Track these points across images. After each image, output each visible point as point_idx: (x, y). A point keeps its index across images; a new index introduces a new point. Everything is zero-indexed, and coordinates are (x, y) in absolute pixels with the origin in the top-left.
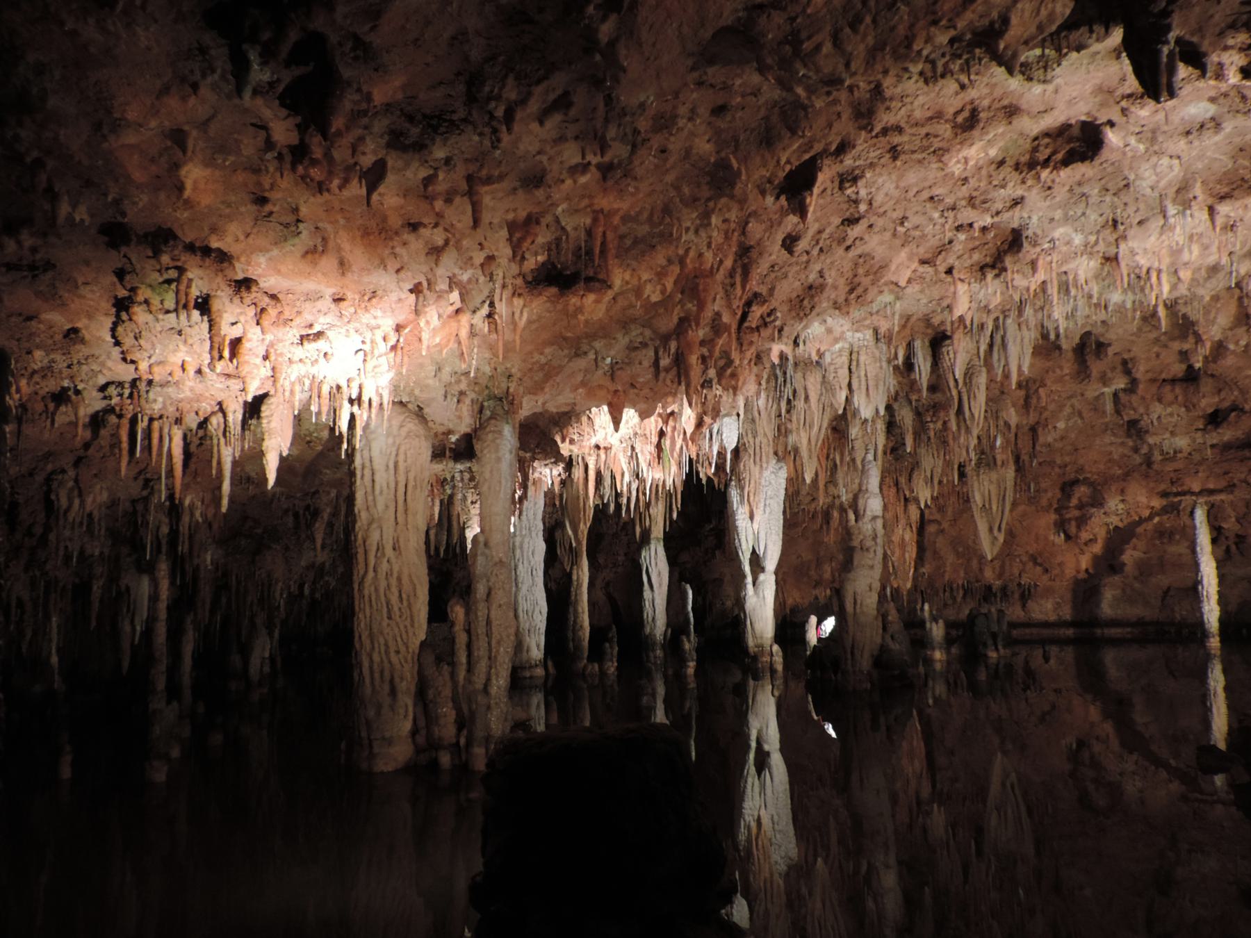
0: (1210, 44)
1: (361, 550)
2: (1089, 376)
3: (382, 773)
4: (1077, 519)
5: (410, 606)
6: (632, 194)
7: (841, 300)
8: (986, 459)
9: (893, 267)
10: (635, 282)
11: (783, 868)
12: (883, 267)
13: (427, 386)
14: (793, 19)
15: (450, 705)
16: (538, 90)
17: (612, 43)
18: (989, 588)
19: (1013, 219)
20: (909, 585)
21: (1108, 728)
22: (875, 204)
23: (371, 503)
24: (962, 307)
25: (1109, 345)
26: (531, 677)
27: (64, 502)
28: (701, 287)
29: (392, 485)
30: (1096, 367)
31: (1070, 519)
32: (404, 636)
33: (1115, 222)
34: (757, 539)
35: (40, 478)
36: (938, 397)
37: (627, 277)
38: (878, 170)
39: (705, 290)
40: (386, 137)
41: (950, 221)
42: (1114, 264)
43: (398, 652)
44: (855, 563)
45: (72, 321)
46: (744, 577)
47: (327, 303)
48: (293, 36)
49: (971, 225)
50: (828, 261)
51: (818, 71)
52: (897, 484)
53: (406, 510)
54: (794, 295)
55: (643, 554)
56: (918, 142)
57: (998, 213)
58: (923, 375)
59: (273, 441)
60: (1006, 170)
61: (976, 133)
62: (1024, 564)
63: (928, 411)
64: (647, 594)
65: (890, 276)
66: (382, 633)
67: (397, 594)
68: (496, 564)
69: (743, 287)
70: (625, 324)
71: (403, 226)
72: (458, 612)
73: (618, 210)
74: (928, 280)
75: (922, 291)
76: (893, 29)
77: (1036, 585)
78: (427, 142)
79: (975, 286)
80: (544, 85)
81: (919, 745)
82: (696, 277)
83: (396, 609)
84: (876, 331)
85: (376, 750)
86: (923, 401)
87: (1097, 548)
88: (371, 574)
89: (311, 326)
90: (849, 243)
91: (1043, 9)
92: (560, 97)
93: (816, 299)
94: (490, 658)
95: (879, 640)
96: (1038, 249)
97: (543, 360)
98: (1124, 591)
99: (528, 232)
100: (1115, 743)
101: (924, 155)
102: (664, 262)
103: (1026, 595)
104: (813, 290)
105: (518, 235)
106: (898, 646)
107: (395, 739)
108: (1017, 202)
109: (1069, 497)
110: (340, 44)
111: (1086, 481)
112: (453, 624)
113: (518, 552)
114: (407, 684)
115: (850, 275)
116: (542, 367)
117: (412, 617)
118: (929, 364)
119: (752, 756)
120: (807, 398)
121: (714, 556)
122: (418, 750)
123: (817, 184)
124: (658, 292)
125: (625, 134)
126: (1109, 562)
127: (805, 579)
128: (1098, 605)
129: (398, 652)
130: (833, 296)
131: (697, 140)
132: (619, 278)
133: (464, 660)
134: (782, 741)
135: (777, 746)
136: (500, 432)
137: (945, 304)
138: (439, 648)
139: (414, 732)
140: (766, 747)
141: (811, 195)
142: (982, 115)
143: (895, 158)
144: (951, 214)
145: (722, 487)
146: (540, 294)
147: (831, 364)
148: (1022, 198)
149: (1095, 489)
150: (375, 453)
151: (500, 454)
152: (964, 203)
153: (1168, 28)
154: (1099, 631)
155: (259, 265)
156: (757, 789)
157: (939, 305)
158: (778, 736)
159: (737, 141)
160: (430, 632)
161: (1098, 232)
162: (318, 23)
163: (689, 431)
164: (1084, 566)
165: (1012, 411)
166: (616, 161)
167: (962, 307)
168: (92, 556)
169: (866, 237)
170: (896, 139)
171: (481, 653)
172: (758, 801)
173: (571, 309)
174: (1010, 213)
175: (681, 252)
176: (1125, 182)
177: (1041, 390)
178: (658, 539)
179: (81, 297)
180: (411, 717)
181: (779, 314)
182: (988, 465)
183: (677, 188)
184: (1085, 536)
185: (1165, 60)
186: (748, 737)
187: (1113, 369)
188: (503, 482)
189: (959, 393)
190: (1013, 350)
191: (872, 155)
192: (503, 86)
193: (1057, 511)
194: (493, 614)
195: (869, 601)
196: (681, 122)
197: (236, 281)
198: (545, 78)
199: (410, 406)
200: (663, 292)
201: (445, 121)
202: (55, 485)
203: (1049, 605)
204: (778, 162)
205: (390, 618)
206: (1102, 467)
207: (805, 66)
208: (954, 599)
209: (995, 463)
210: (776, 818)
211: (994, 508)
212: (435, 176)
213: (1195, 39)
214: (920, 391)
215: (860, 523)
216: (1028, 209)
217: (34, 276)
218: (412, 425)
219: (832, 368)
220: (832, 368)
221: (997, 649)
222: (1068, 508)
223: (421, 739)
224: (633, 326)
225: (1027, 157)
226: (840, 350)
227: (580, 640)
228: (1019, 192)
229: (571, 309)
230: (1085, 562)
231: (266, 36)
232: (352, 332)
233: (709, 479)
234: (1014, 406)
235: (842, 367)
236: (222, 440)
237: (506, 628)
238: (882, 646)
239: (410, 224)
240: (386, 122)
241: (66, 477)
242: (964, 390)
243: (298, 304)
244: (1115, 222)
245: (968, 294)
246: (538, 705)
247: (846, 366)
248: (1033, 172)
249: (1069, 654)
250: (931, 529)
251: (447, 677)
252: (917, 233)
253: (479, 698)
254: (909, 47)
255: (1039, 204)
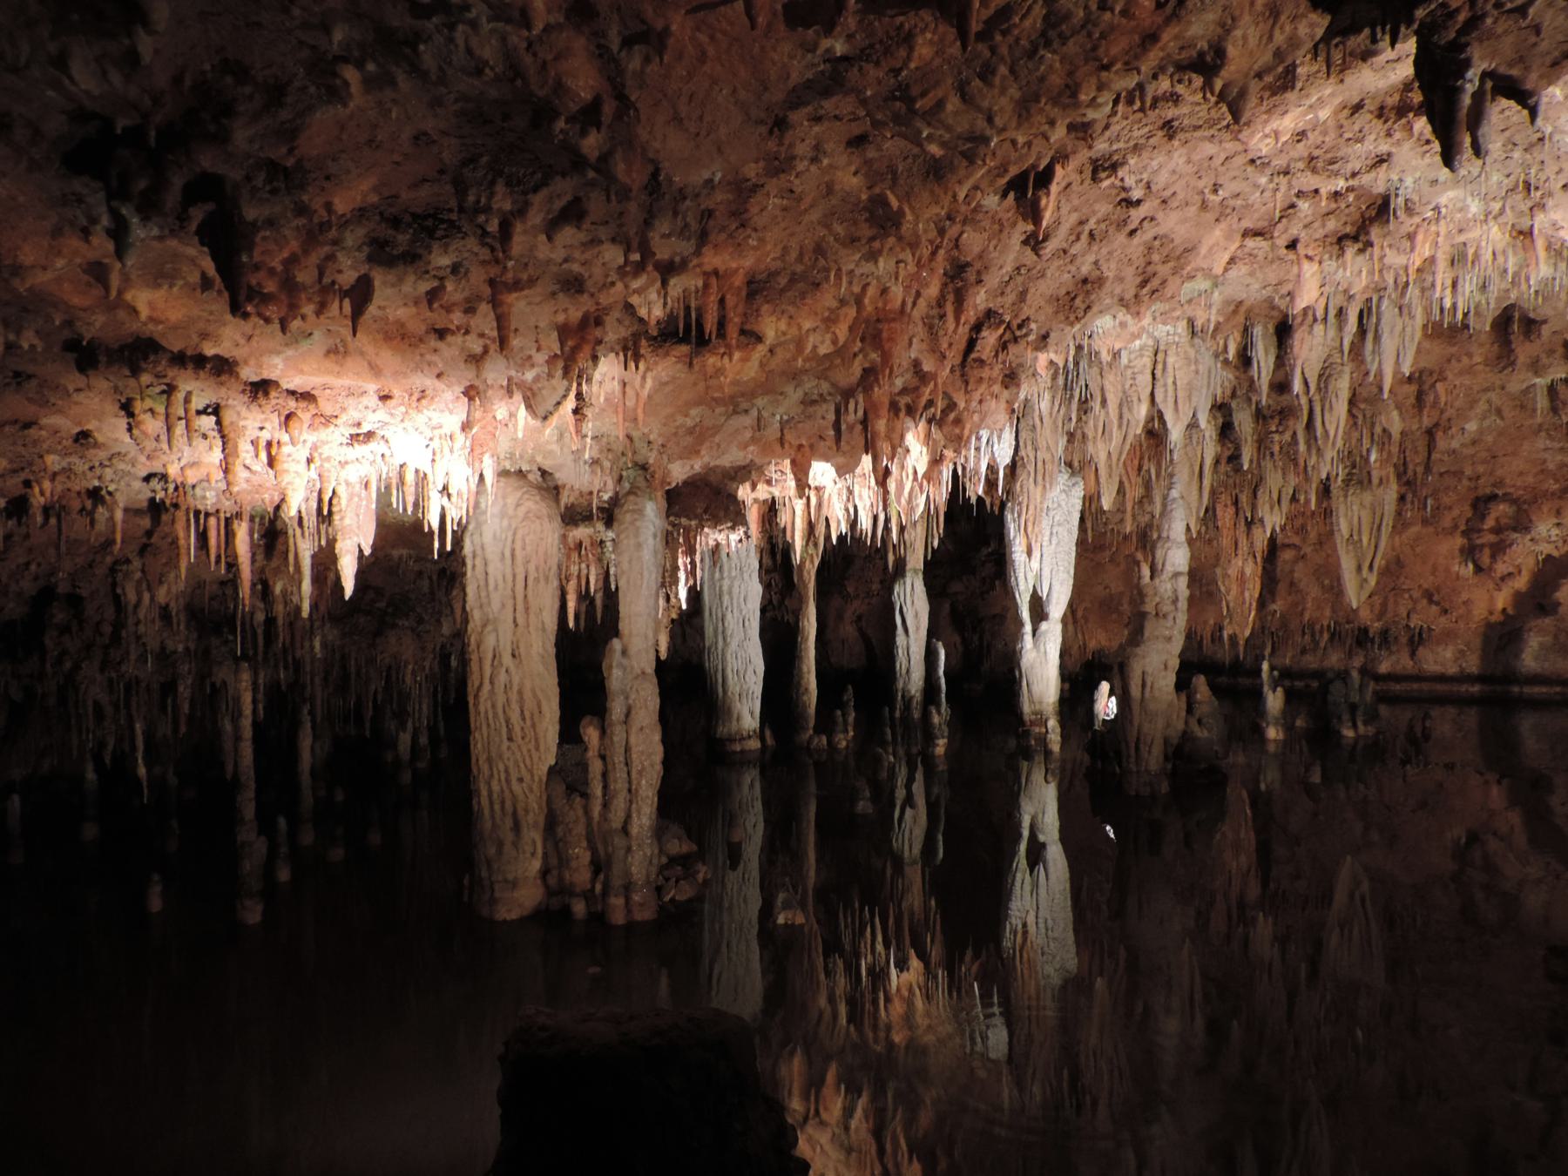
0: (1541, 77)
1: (474, 657)
2: (1513, 363)
3: (505, 921)
4: (1492, 546)
5: (534, 726)
6: (754, 248)
7: (1129, 295)
8: (1358, 476)
9: (1203, 250)
10: (794, 331)
11: (1056, 980)
12: (1189, 250)
13: (551, 452)
14: (896, 72)
15: (584, 844)
16: (537, 199)
17: (605, 158)
18: (1364, 631)
19: (1378, 182)
20: (1247, 633)
21: (1515, 818)
22: (1154, 188)
23: (484, 600)
24: (1309, 295)
25: (1545, 322)
26: (742, 752)
27: (131, 596)
28: (885, 335)
29: (509, 578)
30: (1524, 351)
31: (1483, 546)
32: (528, 762)
33: (1527, 186)
34: (1039, 576)
35: (100, 571)
36: (1285, 400)
37: (783, 326)
38: (1145, 154)
39: (890, 339)
40: (366, 249)
41: (1283, 188)
42: (1527, 241)
43: (521, 780)
44: (1147, 634)
45: (79, 424)
46: (1021, 624)
47: (372, 400)
48: (177, 182)
49: (1316, 191)
50: (1104, 251)
51: (948, 129)
52: (1236, 503)
53: (527, 609)
54: (1063, 291)
55: (896, 589)
56: (1203, 114)
57: (1354, 175)
58: (1264, 374)
59: (348, 542)
60: (1364, 118)
61: (1291, 96)
62: (1415, 602)
63: (1272, 417)
64: (900, 639)
65: (1198, 261)
66: (501, 757)
67: (518, 710)
68: (637, 678)
69: (957, 319)
70: (795, 376)
71: (427, 332)
72: (591, 734)
73: (737, 270)
74: (1261, 258)
75: (1252, 274)
76: (1042, 79)
77: (1430, 629)
78: (420, 251)
79: (1330, 265)
80: (544, 192)
81: (1248, 837)
82: (878, 320)
83: (517, 729)
84: (1191, 323)
85: (497, 895)
86: (1259, 412)
87: (1521, 583)
88: (487, 687)
89: (359, 425)
90: (1132, 227)
91: (1277, 32)
92: (570, 204)
93: (1093, 297)
94: (630, 791)
95: (1180, 726)
96: (1417, 220)
97: (689, 422)
98: (1556, 637)
99: (583, 340)
100: (1520, 839)
101: (1212, 132)
102: (835, 304)
103: (1417, 640)
104: (1089, 284)
105: (570, 343)
106: (1206, 734)
107: (520, 881)
108: (1381, 160)
109: (1483, 517)
110: (248, 178)
111: (1506, 498)
112: (586, 750)
113: (726, 598)
114: (534, 815)
115: (1141, 262)
116: (691, 431)
117: (537, 740)
118: (1272, 359)
119: (1023, 847)
120: (1104, 402)
121: (993, 588)
122: (550, 892)
123: (1055, 181)
124: (828, 342)
125: (686, 225)
126: (1538, 599)
127: (1114, 616)
128: (1517, 655)
129: (521, 780)
130: (1118, 291)
131: (839, 174)
132: (771, 328)
133: (599, 792)
134: (1062, 830)
135: (1056, 835)
136: (640, 512)
137: (1284, 291)
138: (569, 777)
139: (545, 873)
140: (1042, 838)
141: (1048, 194)
142: (1299, 70)
143: (1171, 137)
144: (1283, 180)
145: (996, 509)
146: (667, 354)
147: (1127, 367)
148: (1389, 155)
149: (1519, 509)
150: (488, 538)
151: (641, 539)
152: (1301, 165)
153: (1467, 64)
154: (1516, 689)
155: (275, 366)
156: (1027, 887)
157: (1276, 291)
158: (1057, 824)
159: (895, 174)
160: (561, 754)
161: (1504, 199)
162: (207, 160)
163: (921, 471)
164: (1500, 605)
165: (1395, 413)
166: (677, 259)
167: (1309, 295)
168: (175, 652)
169: (1160, 216)
170: (1170, 112)
171: (619, 786)
172: (1028, 903)
173: (710, 370)
174: (1373, 174)
175: (856, 289)
176: (1539, 135)
177: (1439, 386)
178: (915, 571)
179: (76, 403)
180: (540, 851)
181: (1033, 326)
182: (1360, 482)
183: (828, 227)
184: (1501, 568)
185: (1467, 100)
186: (1019, 825)
187: (1551, 352)
188: (646, 573)
189: (1310, 401)
190: (1389, 344)
191: (1136, 134)
192: (492, 195)
193: (1464, 533)
194: (633, 740)
195: (1162, 683)
196: (801, 166)
197: (252, 384)
198: (544, 183)
199: (531, 477)
200: (835, 342)
201: (442, 221)
202: (120, 576)
203: (1448, 653)
204: (954, 196)
205: (510, 739)
206: (1530, 479)
207: (929, 124)
208: (1317, 643)
209: (1370, 481)
210: (1050, 922)
211: (1365, 540)
212: (442, 288)
213: (1515, 72)
214: (1260, 394)
215: (1157, 581)
216: (1398, 169)
217: (19, 384)
218: (534, 503)
219: (1129, 372)
220: (1129, 372)
221: (1355, 726)
222: (1480, 531)
223: (552, 881)
224: (805, 378)
225: (1397, 97)
226: (1141, 349)
227: (805, 707)
228: (1384, 148)
229: (710, 370)
230: (1502, 600)
231: (142, 184)
232: (411, 430)
233: (980, 499)
234: (1398, 407)
235: (1141, 372)
236: (298, 531)
237: (650, 755)
238: (1185, 732)
239: (436, 331)
240: (361, 232)
241: (131, 567)
242: (1317, 398)
243: (340, 399)
244: (1527, 186)
245: (1318, 276)
246: (752, 786)
247: (1149, 371)
248: (1404, 121)
249: (1471, 717)
250: (1287, 555)
251: (580, 812)
252: (1239, 202)
253: (616, 840)
254: (1074, 95)
255: (1414, 163)
